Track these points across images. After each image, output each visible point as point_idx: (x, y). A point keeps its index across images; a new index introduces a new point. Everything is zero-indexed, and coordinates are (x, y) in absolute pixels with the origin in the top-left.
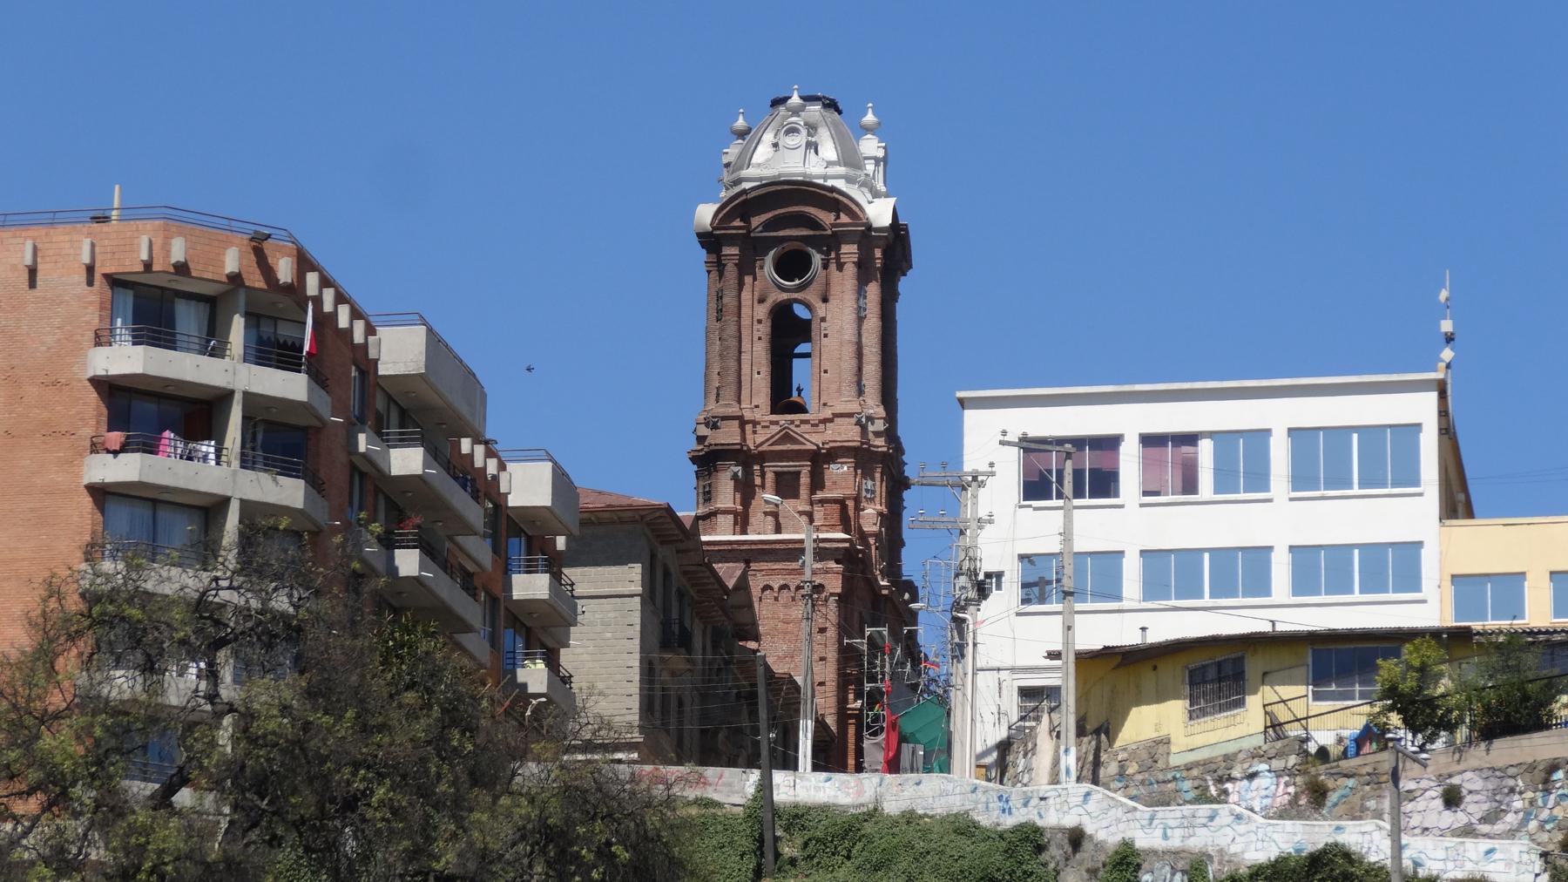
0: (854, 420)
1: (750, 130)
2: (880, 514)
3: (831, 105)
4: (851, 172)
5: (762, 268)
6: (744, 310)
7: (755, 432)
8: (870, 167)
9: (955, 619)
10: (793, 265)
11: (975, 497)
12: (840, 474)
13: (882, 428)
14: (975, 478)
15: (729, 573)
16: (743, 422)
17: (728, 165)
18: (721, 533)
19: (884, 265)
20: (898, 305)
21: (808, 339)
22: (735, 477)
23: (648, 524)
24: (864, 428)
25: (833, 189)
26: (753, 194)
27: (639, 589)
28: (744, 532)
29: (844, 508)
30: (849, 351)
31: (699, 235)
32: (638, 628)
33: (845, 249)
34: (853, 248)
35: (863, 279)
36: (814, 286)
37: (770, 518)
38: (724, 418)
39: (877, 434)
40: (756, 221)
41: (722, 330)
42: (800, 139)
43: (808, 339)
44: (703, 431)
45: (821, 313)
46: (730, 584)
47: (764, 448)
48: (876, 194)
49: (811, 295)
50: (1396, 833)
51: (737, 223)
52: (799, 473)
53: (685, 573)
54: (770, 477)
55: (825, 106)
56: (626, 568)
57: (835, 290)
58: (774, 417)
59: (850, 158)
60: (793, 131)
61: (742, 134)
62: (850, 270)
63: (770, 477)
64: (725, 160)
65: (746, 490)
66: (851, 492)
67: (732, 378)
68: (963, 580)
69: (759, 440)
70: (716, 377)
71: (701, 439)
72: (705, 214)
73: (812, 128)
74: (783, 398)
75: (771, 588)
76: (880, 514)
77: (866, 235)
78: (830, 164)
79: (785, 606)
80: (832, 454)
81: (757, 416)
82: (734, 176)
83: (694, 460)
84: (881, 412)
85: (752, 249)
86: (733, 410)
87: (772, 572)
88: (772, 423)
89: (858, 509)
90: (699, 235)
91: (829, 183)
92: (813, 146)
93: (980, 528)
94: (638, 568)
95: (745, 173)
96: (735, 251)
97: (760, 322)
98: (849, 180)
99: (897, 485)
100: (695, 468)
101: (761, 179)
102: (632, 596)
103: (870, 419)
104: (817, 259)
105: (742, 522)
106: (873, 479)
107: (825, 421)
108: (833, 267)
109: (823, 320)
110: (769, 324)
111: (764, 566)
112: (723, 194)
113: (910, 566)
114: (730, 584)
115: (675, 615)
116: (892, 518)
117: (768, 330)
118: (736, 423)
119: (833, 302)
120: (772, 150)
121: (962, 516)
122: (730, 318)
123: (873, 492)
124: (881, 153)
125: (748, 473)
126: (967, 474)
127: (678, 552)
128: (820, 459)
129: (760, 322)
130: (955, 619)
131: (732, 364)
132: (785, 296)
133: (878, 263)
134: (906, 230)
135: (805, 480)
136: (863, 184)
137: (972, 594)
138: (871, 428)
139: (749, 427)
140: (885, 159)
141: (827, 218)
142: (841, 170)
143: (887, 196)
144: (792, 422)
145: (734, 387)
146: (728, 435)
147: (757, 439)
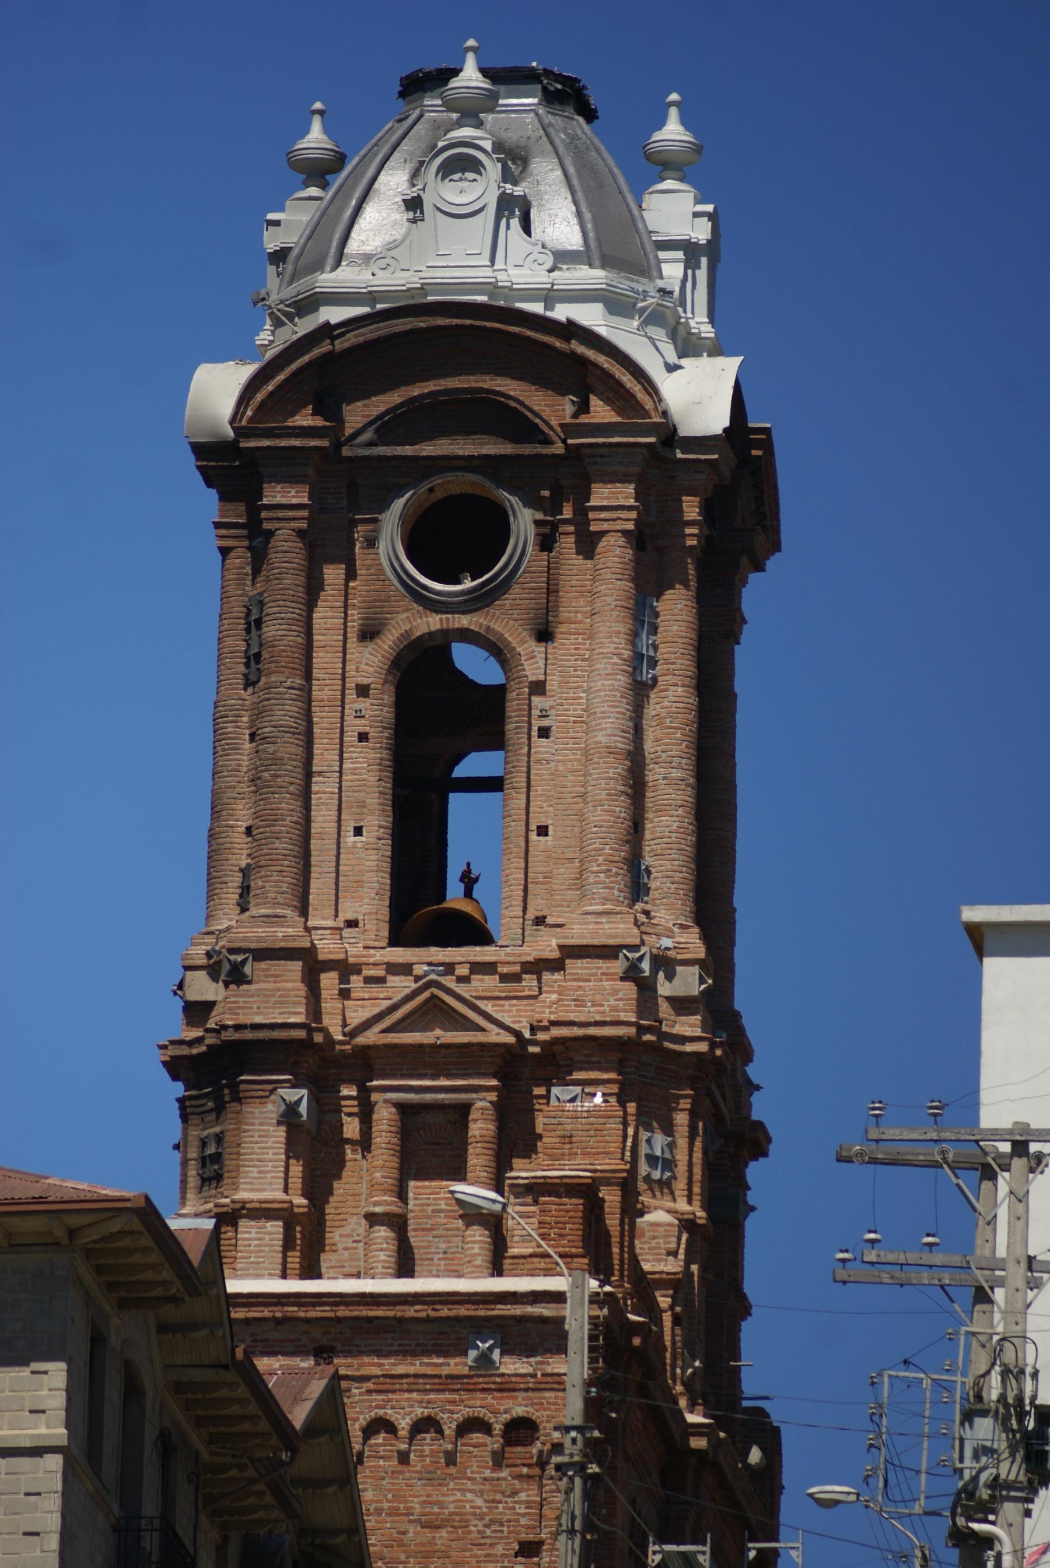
0: (618, 966)
1: (339, 160)
2: (687, 1224)
3: (567, 95)
4: (623, 284)
5: (371, 543)
6: (320, 659)
7: (345, 994)
8: (673, 270)
9: (961, 1538)
10: (457, 539)
11: (1020, 1197)
12: (581, 1114)
13: (695, 989)
14: (1020, 1148)
15: (294, 1382)
16: (313, 966)
17: (279, 256)
18: (255, 1276)
19: (708, 543)
20: (739, 651)
21: (496, 741)
22: (289, 1116)
23: (89, 1253)
24: (646, 988)
25: (571, 330)
26: (352, 339)
27: (55, 1431)
28: (311, 1271)
29: (594, 1208)
30: (607, 776)
31: (199, 450)
32: (53, 1542)
33: (601, 495)
34: (625, 494)
35: (648, 582)
36: (515, 592)
37: (383, 1232)
38: (263, 954)
39: (682, 1005)
40: (357, 415)
41: (259, 712)
42: (483, 189)
43: (496, 741)
44: (202, 987)
45: (532, 671)
46: (299, 1416)
47: (371, 1037)
48: (688, 346)
49: (505, 621)
50: (49, 1533)
51: (305, 419)
52: (465, 1109)
53: (178, 1387)
54: (384, 1116)
55: (551, 98)
56: (24, 1372)
57: (572, 607)
58: (400, 955)
59: (617, 243)
60: (461, 164)
61: (319, 171)
62: (614, 552)
63: (384, 1116)
64: (272, 241)
65: (318, 1152)
66: (611, 1163)
67: (284, 846)
68: (984, 1429)
69: (358, 1014)
70: (238, 839)
71: (197, 1011)
72: (217, 390)
73: (514, 159)
74: (424, 904)
75: (389, 1427)
76: (687, 1224)
77: (660, 454)
78: (563, 258)
79: (428, 1478)
80: (558, 1058)
81: (351, 947)
82: (301, 285)
83: (175, 1068)
84: (692, 943)
85: (347, 490)
86: (288, 932)
87: (389, 1384)
88: (394, 969)
89: (631, 1210)
90: (199, 450)
91: (561, 313)
92: (516, 210)
93: (1035, 1285)
94: (57, 1373)
95: (327, 280)
96: (296, 495)
97: (363, 691)
98: (616, 305)
99: (734, 1143)
100: (178, 1089)
101: (371, 297)
102: (37, 1452)
103: (664, 963)
104: (524, 521)
105: (306, 1241)
106: (668, 1129)
107: (538, 967)
108: (567, 543)
109: (538, 688)
110: (388, 698)
111: (372, 1366)
112: (264, 337)
113: (765, 1365)
114: (299, 1416)
115: (150, 1506)
116: (718, 1234)
117: (387, 713)
118: (297, 966)
119: (565, 642)
120: (401, 216)
121: (982, 1251)
122: (282, 680)
123: (669, 1164)
124: (702, 232)
125: (326, 1105)
126: (997, 1135)
127: (162, 1328)
128: (525, 1070)
129: (363, 691)
130: (961, 1538)
131: (287, 806)
132: (434, 622)
133: (692, 536)
134: (767, 445)
135: (481, 1127)
136: (654, 318)
137: (1011, 1469)
138: (664, 988)
139: (329, 981)
140: (712, 249)
141: (553, 409)
142: (592, 276)
143: (717, 350)
144: (449, 968)
145: (289, 867)
146: (272, 1002)
147: (352, 1013)
